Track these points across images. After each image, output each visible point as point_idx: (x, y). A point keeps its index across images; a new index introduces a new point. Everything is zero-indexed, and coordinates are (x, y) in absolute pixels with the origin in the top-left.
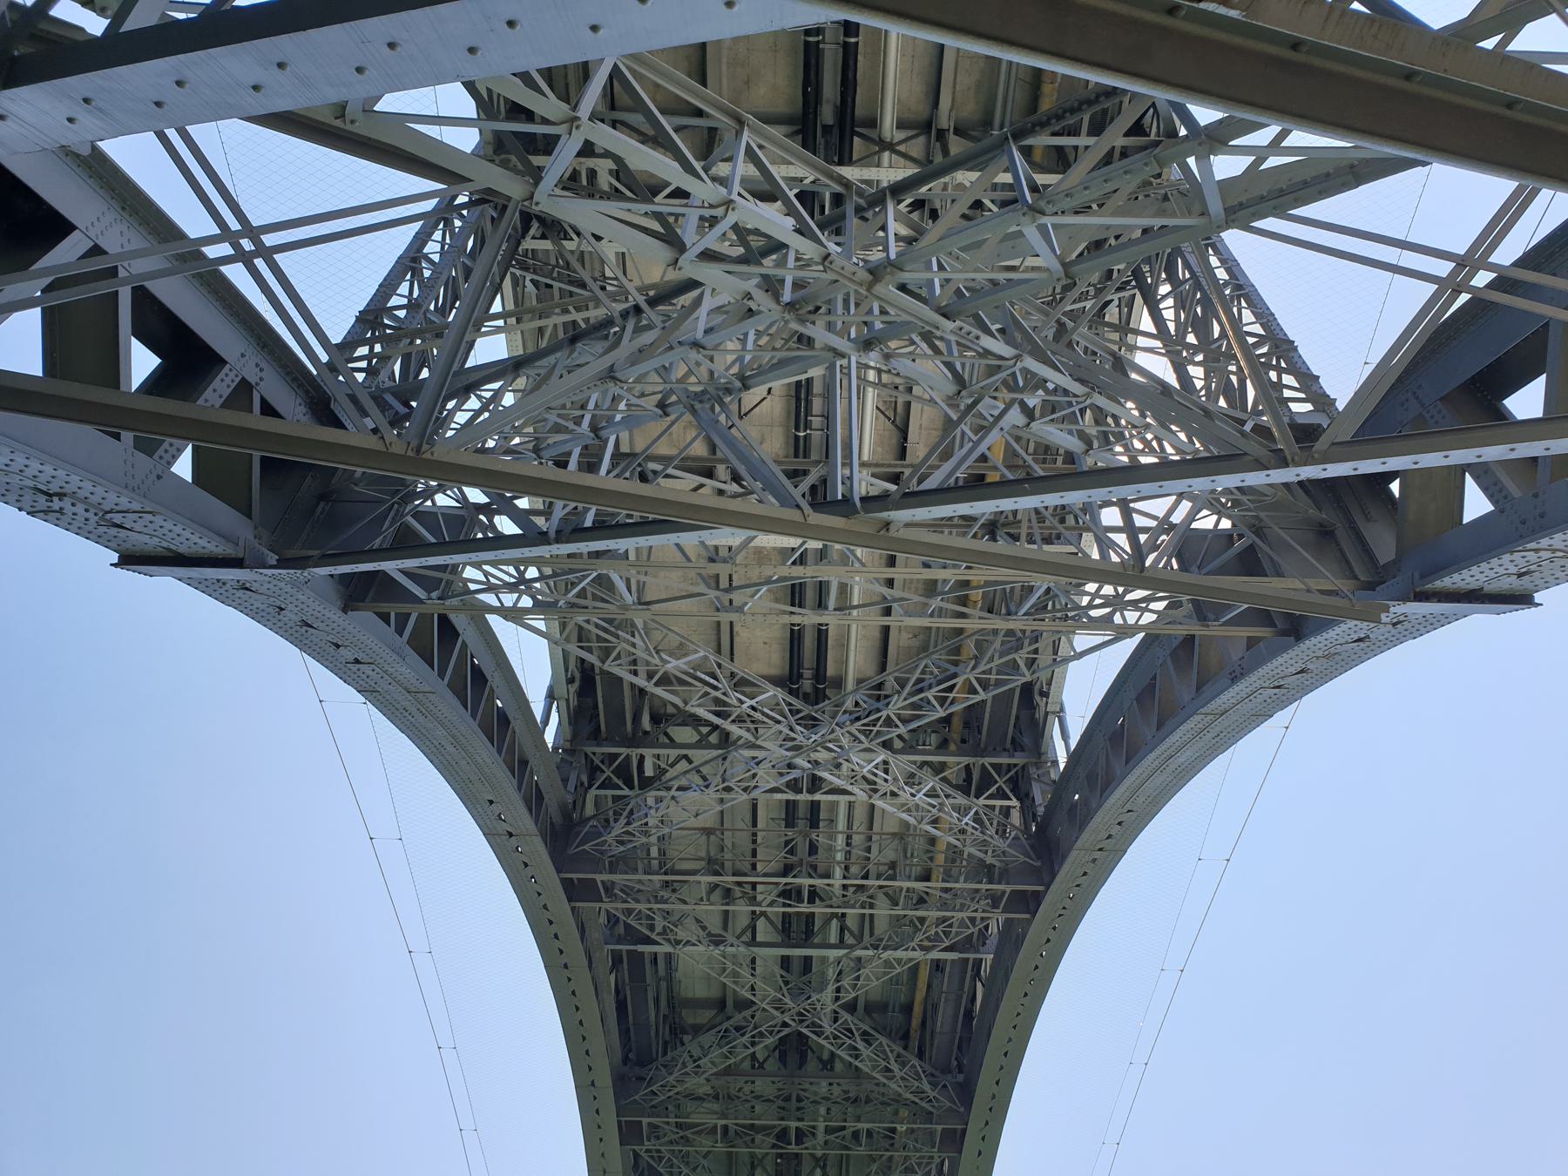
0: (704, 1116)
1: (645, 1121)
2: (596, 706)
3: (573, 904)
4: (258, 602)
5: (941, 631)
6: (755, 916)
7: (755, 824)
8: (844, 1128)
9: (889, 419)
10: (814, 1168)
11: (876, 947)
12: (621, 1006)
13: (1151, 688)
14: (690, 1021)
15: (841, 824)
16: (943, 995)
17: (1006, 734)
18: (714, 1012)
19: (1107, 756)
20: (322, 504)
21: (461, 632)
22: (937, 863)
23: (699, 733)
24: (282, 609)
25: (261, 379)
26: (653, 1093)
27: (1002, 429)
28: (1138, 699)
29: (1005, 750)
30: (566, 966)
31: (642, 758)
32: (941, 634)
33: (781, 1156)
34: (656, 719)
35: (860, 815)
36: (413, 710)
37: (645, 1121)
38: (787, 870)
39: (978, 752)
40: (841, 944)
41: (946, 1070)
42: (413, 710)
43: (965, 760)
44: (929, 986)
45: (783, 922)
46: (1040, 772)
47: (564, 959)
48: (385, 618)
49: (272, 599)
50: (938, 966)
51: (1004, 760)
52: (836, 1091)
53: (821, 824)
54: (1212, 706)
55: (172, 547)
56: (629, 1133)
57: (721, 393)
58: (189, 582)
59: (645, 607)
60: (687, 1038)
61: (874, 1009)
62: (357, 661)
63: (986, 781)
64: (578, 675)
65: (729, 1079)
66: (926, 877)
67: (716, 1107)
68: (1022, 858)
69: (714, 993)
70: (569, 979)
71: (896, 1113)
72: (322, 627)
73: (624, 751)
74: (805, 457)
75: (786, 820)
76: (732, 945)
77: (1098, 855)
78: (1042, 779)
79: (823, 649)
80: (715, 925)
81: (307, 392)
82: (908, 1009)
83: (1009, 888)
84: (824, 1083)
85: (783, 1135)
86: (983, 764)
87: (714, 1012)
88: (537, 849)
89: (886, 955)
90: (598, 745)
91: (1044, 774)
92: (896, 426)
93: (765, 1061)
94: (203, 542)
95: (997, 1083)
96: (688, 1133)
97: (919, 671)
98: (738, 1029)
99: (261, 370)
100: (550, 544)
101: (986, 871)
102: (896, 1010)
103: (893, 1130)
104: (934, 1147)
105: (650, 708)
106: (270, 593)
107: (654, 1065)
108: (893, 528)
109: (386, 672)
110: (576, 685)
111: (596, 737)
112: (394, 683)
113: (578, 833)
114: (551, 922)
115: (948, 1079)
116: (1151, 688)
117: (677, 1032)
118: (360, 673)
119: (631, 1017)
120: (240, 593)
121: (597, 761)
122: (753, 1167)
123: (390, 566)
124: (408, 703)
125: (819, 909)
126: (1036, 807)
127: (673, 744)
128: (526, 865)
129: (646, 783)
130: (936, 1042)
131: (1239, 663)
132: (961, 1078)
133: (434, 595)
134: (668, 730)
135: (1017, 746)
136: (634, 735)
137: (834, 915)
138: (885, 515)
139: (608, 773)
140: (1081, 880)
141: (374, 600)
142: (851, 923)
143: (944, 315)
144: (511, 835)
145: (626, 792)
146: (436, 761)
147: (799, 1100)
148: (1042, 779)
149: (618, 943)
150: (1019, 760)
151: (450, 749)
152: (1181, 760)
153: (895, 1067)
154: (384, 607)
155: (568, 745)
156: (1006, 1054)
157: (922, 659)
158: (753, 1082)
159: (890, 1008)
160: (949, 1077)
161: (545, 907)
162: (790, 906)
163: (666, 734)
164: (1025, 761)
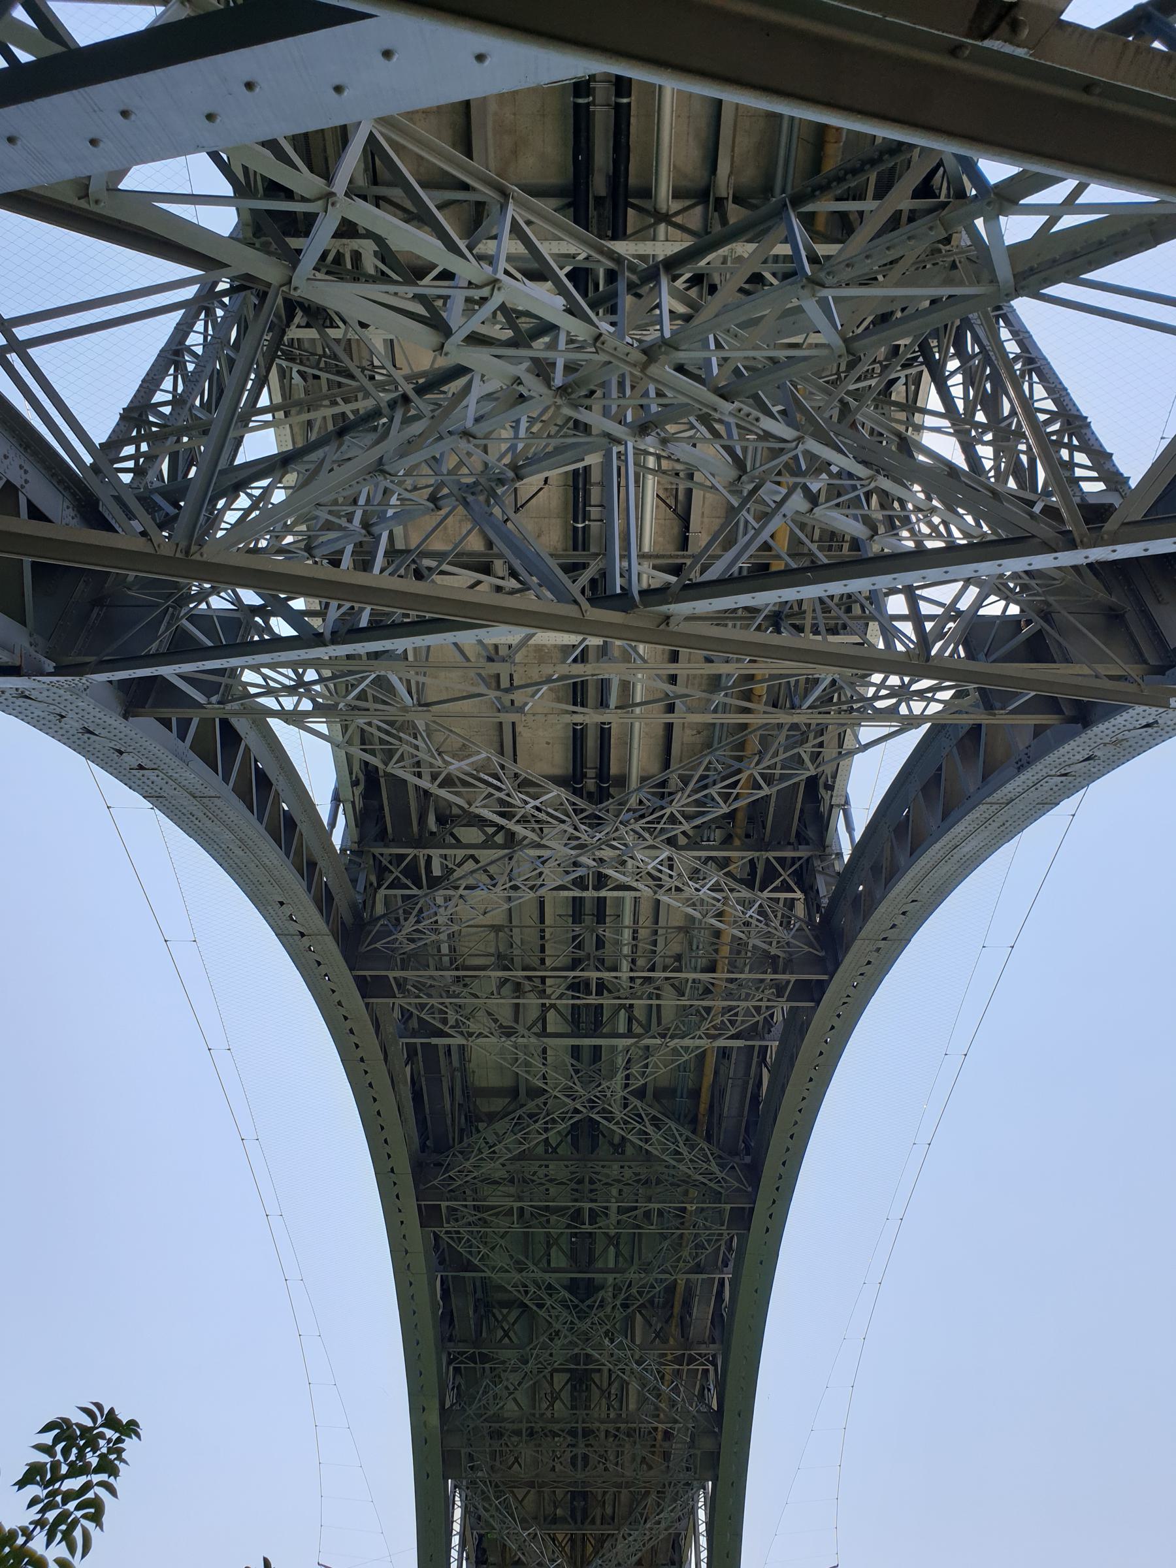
1: (444, 1204)
7: (542, 921)
10: (608, 1246)
11: (663, 1036)
12: (417, 1097)
13: (937, 778)
15: (628, 920)
18: (507, 1100)
19: (892, 848)
20: (96, 610)
21: (242, 735)
23: (485, 833)
24: (63, 717)
25: (26, 481)
29: (789, 844)
30: (362, 1060)
33: (575, 1234)
34: (441, 820)
36: (200, 815)
38: (575, 964)
39: (763, 846)
40: (630, 1033)
41: (734, 1153)
42: (200, 815)
43: (750, 855)
44: (716, 1073)
45: (573, 1014)
46: (824, 864)
48: (166, 723)
50: (724, 1053)
51: (789, 854)
52: (628, 1173)
53: (608, 919)
54: (998, 795)
56: (429, 1216)
57: (493, 484)
59: (425, 708)
60: (481, 1126)
61: (662, 1094)
62: (141, 767)
63: (771, 874)
64: (362, 777)
66: (712, 968)
68: (807, 949)
69: (508, 1082)
70: (366, 1072)
71: (686, 1193)
72: (104, 733)
76: (523, 1036)
77: (882, 944)
78: (827, 871)
81: (74, 495)
82: (696, 1094)
83: (793, 978)
84: (616, 1166)
85: (577, 1215)
86: (767, 858)
89: (674, 1043)
90: (386, 846)
91: (828, 867)
92: (678, 515)
97: (702, 768)
99: (26, 472)
100: (325, 645)
101: (773, 963)
103: (684, 1210)
109: (170, 777)
111: (382, 837)
112: (178, 788)
114: (346, 1018)
117: (472, 1119)
119: (427, 1106)
120: (20, 702)
122: (549, 1246)
125: (607, 1001)
127: (459, 844)
129: (434, 883)
130: (724, 1125)
131: (1026, 751)
132: (748, 1159)
133: (214, 699)
135: (801, 839)
138: (664, 608)
139: (397, 873)
143: (722, 396)
144: (302, 935)
146: (225, 865)
147: (592, 1182)
148: (827, 871)
150: (803, 853)
151: (239, 852)
153: (684, 1150)
154: (165, 712)
156: (792, 1137)
157: (706, 755)
158: (547, 1166)
160: (737, 1159)
161: (340, 1003)
162: (578, 998)
163: (452, 835)
164: (809, 854)
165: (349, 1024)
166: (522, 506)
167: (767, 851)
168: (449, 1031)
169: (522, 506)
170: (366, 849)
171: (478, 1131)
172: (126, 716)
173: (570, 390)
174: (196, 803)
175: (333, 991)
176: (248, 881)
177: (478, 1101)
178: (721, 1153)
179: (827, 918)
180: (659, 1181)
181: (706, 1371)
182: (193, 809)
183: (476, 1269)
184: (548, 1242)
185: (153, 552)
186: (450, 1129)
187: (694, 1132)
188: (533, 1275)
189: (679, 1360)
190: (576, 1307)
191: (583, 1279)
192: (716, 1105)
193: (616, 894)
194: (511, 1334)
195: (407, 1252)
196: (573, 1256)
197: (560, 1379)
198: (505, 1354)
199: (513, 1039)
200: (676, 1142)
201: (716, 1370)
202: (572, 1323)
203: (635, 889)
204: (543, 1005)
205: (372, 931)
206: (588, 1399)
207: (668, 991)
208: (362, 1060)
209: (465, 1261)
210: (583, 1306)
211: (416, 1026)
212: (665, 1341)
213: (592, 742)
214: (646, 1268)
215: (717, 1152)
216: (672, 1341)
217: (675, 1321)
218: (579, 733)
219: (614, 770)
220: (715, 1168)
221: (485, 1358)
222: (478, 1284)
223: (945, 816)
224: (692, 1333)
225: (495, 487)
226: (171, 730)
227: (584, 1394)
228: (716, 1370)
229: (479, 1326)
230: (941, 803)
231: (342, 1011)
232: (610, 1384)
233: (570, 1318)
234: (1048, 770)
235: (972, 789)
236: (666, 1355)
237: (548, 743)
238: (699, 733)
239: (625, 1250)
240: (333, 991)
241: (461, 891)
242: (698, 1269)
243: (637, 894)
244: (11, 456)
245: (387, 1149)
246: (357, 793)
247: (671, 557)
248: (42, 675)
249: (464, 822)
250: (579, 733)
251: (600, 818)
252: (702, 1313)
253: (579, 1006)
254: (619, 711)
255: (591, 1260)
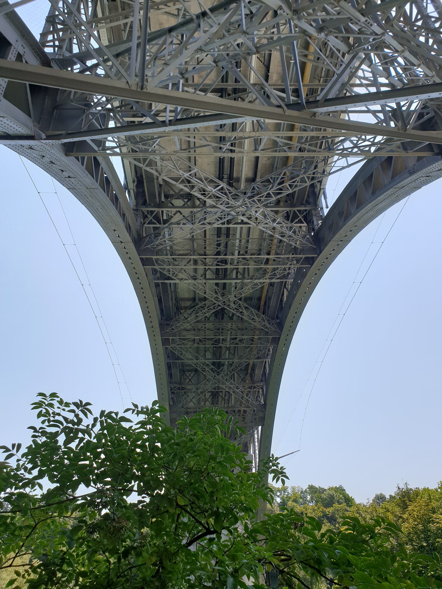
0: (190, 336)
1: (170, 338)
2: (144, 192)
3: (144, 267)
4: (34, 154)
5: (280, 158)
6: (205, 270)
7: (205, 237)
8: (236, 338)
9: (262, 62)
10: (226, 351)
11: (251, 279)
12: (160, 301)
13: (371, 177)
14: (183, 305)
15: (238, 236)
16: (273, 294)
17: (303, 198)
18: (191, 302)
19: (348, 205)
20: (55, 111)
21: (101, 163)
22: (273, 248)
23: (184, 201)
24: (43, 156)
25: (25, 52)
26: (173, 329)
27: (351, 68)
28: (364, 182)
29: (303, 204)
30: (142, 288)
31: (162, 211)
32: (280, 159)
33: (215, 347)
34: (166, 197)
35: (245, 231)
36: (88, 196)
37: (170, 338)
38: (218, 253)
39: (292, 205)
40: (237, 278)
41: (273, 319)
42: (88, 196)
43: (288, 209)
44: (267, 291)
45: (216, 272)
46: (316, 212)
47: (141, 286)
48: (77, 158)
49: (41, 153)
50: (271, 284)
51: (302, 208)
52: (234, 326)
53: (230, 236)
54: (400, 185)
55: (7, 132)
56: (165, 342)
57: (245, 55)
58: (9, 146)
59: (184, 151)
60: (182, 311)
61: (247, 299)
62: (69, 177)
63: (295, 216)
64: (136, 179)
65: (198, 324)
66: (269, 254)
67: (193, 332)
68: (310, 245)
69: (191, 296)
70: (143, 293)
71: (254, 332)
72: (58, 163)
73: (156, 210)
74: (226, 82)
75: (227, 234)
76: (200, 280)
77: (340, 243)
78: (317, 215)
79: (232, 165)
80: (192, 274)
81: (41, 58)
82: (259, 299)
83: (304, 256)
84: (230, 324)
85: (217, 341)
86: (294, 211)
87: (191, 302)
88: (132, 247)
89: (256, 281)
90: (147, 207)
91: (317, 213)
92: (265, 65)
93: (210, 318)
94: (20, 129)
95: (292, 322)
96: (185, 341)
97: (282, 174)
98: (202, 307)
99: (24, 48)
100: (166, 126)
101: (295, 250)
102: (256, 299)
103: (254, 338)
104: (269, 343)
105: (164, 192)
106: (41, 150)
107: (173, 320)
108: (316, 115)
109: (80, 181)
110: (136, 183)
111: (145, 203)
112: (82, 185)
113: (145, 241)
114: (136, 273)
115: (274, 322)
116: (371, 177)
117: (178, 308)
118: (70, 182)
119: (163, 305)
120: (28, 151)
121: (146, 213)
122: (205, 351)
123: (87, 139)
124: (87, 193)
125: (228, 266)
126: (314, 226)
127: (173, 206)
128: (127, 253)
129: (165, 222)
130: (270, 310)
131: (413, 167)
132: (278, 321)
133: (100, 148)
134: (172, 202)
135: (308, 203)
136: (160, 203)
137: (234, 269)
138: (315, 110)
139: (151, 218)
140: (331, 252)
141: (76, 152)
142: (241, 270)
143: (362, 15)
144: (122, 242)
145: (158, 225)
146: (95, 215)
147: (223, 329)
148: (317, 215)
149: (158, 280)
150: (308, 208)
151: (101, 210)
152: (380, 206)
153: (256, 317)
154: (80, 155)
155: (135, 208)
156: (296, 313)
157: (284, 169)
158: (205, 325)
159: (253, 299)
160: (274, 320)
161: (134, 268)
162: (223, 266)
163: (171, 203)
164: (311, 208)
165: (137, 276)
166: (200, 62)
167: (294, 207)
168: (174, 278)
169: (200, 62)
170: (139, 208)
171: (181, 313)
172: (66, 155)
173: (299, 12)
174: (88, 191)
175: (132, 263)
176: (103, 222)
177: (181, 303)
178: (269, 319)
179: (316, 234)
180: (246, 329)
181: (259, 391)
182: (86, 193)
183: (181, 359)
184: (205, 350)
185: (128, 88)
186: (172, 312)
187: (259, 311)
188: (201, 361)
189: (250, 388)
190: (216, 371)
191: (217, 362)
192: (267, 302)
193: (235, 226)
194: (192, 380)
195: (157, 354)
196: (214, 354)
197: (208, 395)
198: (189, 387)
199: (197, 281)
200: (253, 315)
201: (263, 391)
202: (215, 376)
203: (249, 224)
204: (205, 268)
205: (145, 241)
206: (218, 401)
207: (252, 263)
208: (142, 288)
209: (177, 356)
210: (219, 371)
211: (159, 276)
212: (245, 382)
213: (227, 164)
214: (241, 357)
215: (268, 318)
216: (247, 381)
217: (249, 375)
218: (222, 161)
219: (235, 175)
220: (266, 323)
221: (183, 389)
222: (180, 364)
223: (373, 193)
224: (255, 379)
225: (246, 57)
226: (79, 161)
227: (216, 399)
228: (263, 391)
229: (181, 378)
230: (372, 187)
231: (135, 271)
232: (225, 396)
233: (214, 375)
234: (422, 175)
235: (386, 182)
236: (245, 386)
237: (208, 164)
238: (269, 159)
239: (232, 352)
240: (132, 263)
241: (181, 225)
242: (258, 358)
243: (248, 226)
244: (19, 40)
245: (151, 319)
246: (135, 185)
247: (280, 85)
248: (42, 140)
249: (176, 197)
250: (222, 161)
251: (238, 195)
252: (258, 373)
253: (218, 269)
254: (262, 151)
255: (220, 356)
